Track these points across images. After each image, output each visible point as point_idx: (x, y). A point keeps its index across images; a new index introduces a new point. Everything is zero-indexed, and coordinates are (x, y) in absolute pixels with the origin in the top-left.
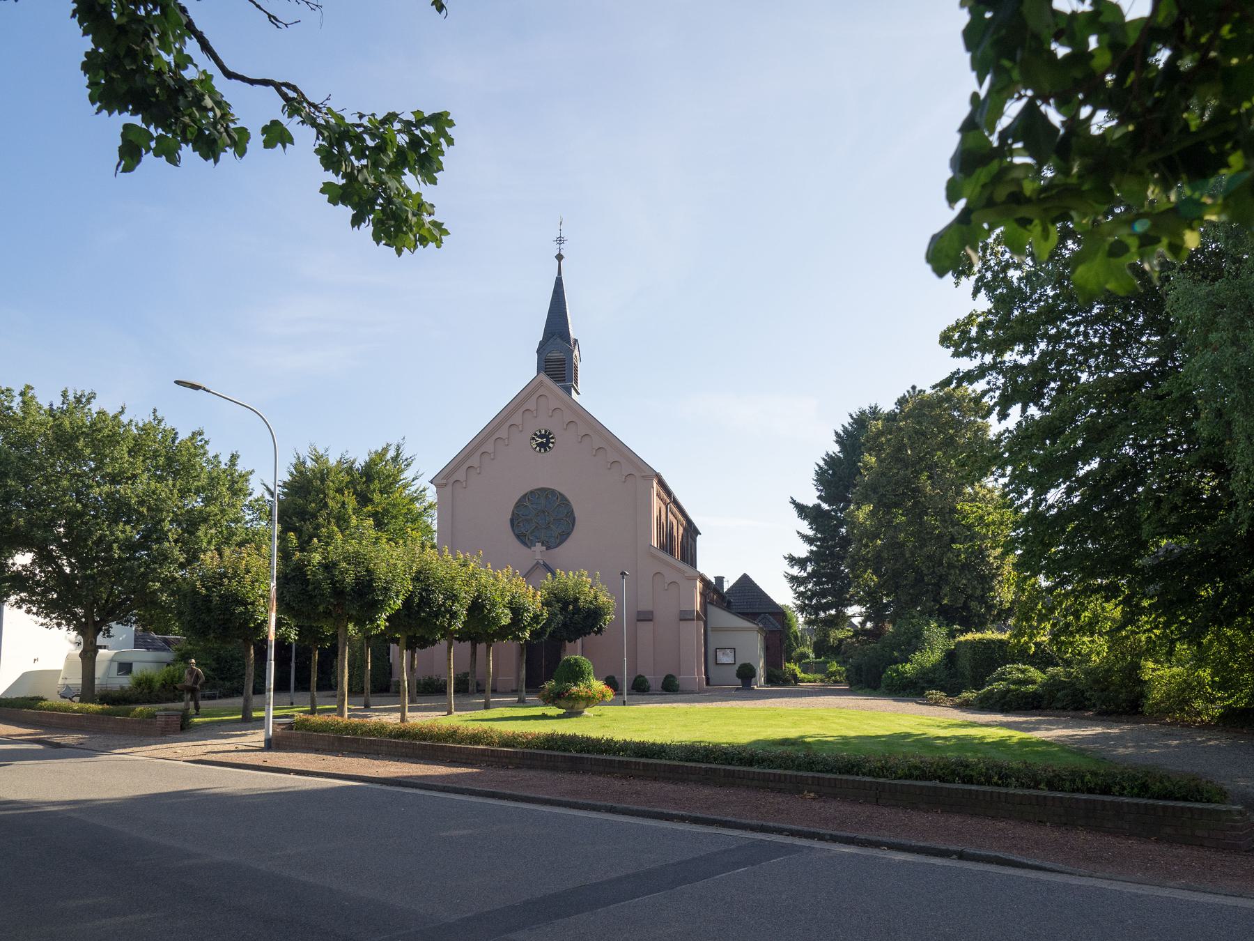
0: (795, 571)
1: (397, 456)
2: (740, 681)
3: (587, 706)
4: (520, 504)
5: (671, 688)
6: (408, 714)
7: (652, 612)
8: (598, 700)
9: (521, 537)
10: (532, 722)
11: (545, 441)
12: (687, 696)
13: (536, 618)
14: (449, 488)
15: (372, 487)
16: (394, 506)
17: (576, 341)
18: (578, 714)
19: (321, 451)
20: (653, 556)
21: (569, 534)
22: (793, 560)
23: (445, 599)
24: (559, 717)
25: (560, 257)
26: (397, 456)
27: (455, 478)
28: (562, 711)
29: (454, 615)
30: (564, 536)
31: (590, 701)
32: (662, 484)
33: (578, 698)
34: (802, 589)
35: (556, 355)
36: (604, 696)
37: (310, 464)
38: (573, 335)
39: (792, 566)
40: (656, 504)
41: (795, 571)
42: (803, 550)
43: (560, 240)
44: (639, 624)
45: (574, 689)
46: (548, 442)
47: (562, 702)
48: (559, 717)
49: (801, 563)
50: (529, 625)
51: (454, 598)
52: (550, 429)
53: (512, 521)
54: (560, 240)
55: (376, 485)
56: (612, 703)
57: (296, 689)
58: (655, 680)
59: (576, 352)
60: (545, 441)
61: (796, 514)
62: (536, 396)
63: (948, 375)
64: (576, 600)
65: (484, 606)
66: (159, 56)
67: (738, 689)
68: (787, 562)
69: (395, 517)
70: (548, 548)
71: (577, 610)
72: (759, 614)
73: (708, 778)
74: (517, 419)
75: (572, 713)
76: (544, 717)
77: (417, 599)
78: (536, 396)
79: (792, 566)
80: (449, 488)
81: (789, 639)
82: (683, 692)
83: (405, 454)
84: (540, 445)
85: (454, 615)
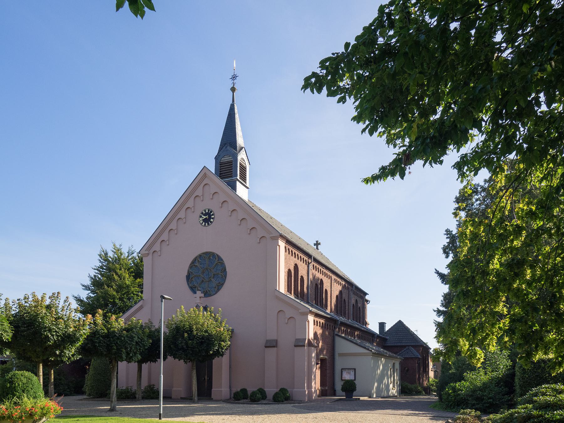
2: (344, 393)
7: (276, 341)
9: (193, 289)
11: (208, 217)
19: (118, 247)
21: (223, 284)
25: (233, 90)
27: (154, 249)
32: (288, 242)
35: (226, 159)
37: (111, 254)
39: (439, 316)
43: (234, 77)
44: (266, 349)
46: (210, 218)
53: (188, 278)
54: (234, 77)
58: (271, 390)
60: (208, 217)
61: (440, 281)
64: (191, 330)
66: (464, 256)
68: (435, 313)
70: (207, 294)
71: (191, 337)
72: (405, 346)
74: (190, 204)
80: (150, 256)
84: (205, 220)
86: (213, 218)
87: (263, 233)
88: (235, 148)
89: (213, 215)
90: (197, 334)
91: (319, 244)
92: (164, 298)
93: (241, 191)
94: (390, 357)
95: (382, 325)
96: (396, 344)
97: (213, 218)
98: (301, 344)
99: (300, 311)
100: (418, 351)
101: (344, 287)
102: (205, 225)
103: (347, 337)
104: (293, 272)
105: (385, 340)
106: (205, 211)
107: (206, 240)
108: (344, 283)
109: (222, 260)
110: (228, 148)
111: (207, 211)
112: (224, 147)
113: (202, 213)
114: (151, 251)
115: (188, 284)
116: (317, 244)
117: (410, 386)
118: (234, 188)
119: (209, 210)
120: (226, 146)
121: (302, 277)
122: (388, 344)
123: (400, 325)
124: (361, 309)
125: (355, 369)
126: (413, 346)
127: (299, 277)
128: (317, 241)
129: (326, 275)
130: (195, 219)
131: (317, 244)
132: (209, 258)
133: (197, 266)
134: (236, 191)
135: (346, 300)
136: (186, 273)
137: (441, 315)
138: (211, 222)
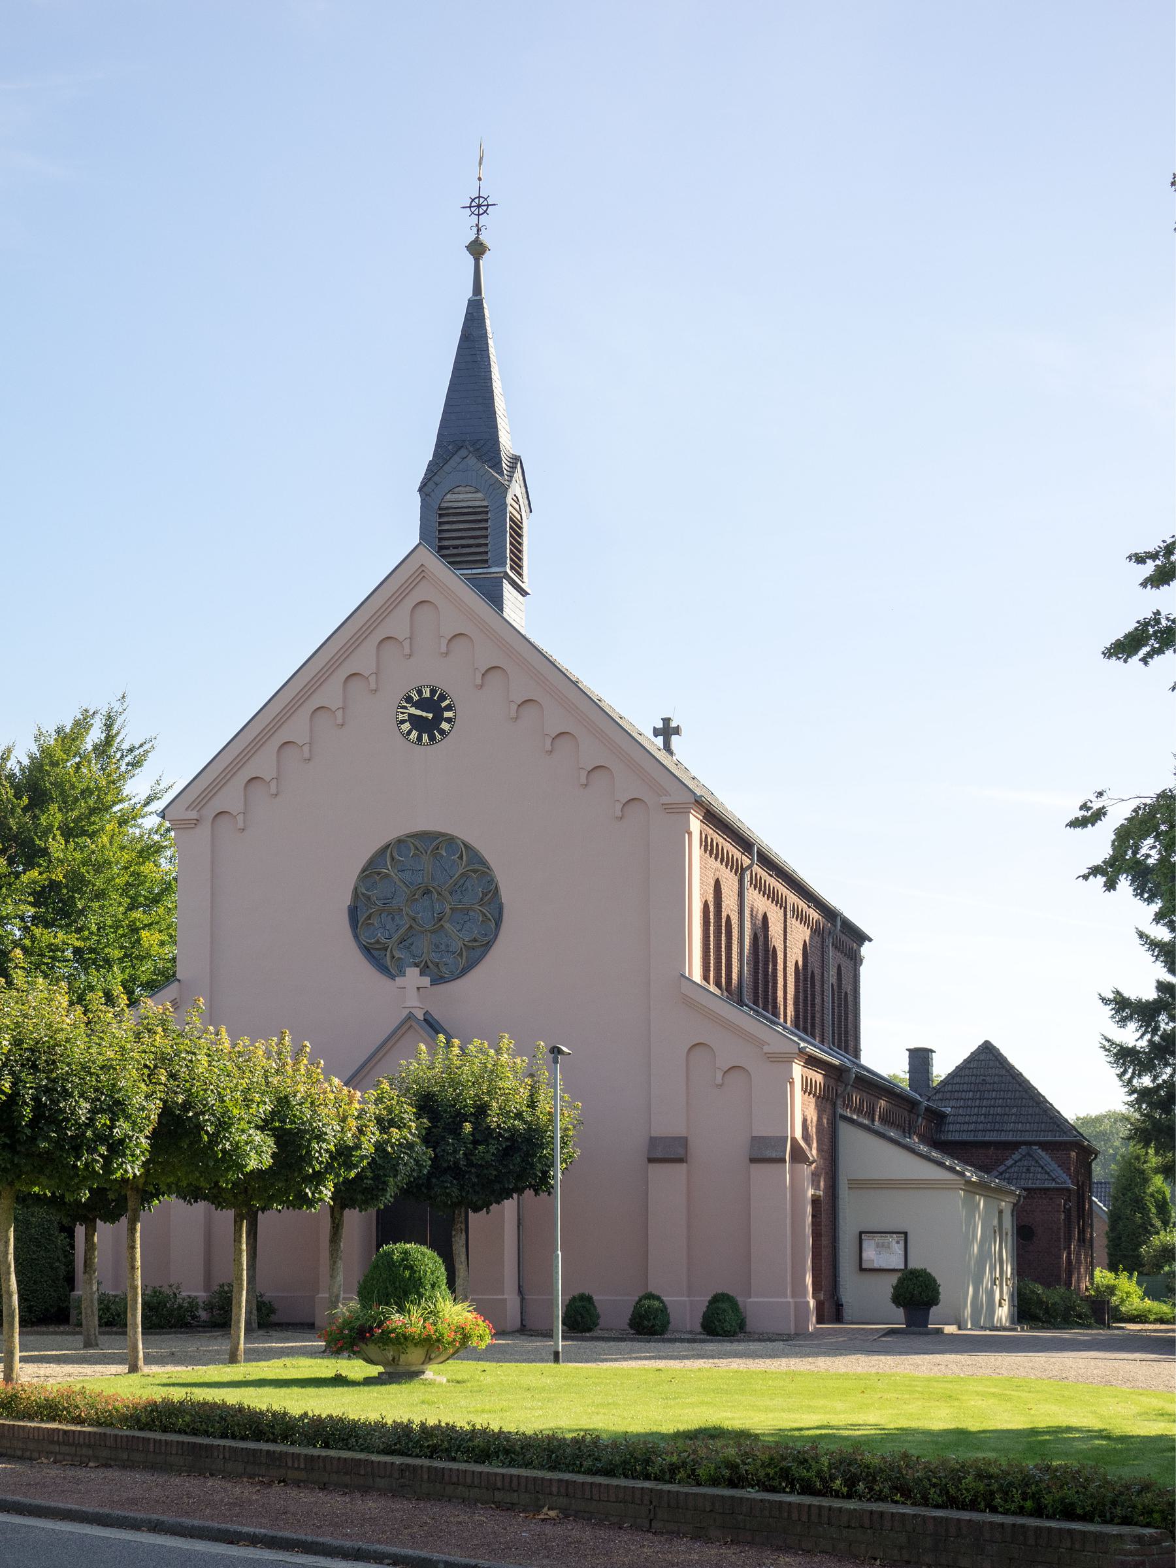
0: (1131, 1035)
1: (109, 741)
2: (901, 1311)
3: (428, 1359)
4: (371, 871)
5: (724, 1324)
6: (17, 1365)
7: (684, 1142)
8: (461, 1346)
9: (374, 953)
10: (311, 1391)
11: (429, 716)
12: (753, 1346)
13: (343, 1154)
14: (205, 830)
15: (44, 820)
16: (99, 868)
17: (516, 460)
18: (412, 1375)
20: (689, 1003)
21: (488, 946)
22: (1123, 1007)
23: (94, 1112)
24: (368, 1382)
25: (477, 249)
26: (109, 741)
27: (217, 805)
28: (374, 1370)
29: (117, 1148)
30: (477, 950)
31: (432, 1347)
32: (715, 819)
33: (403, 1340)
34: (1146, 1081)
35: (464, 498)
36: (466, 1337)
38: (508, 442)
39: (1123, 1022)
40: (700, 873)
41: (1131, 1035)
42: (1144, 978)
43: (479, 206)
45: (397, 1320)
46: (439, 718)
47: (372, 1350)
48: (368, 1382)
49: (1145, 1013)
50: (329, 1167)
51: (117, 1108)
52: (444, 685)
53: (353, 912)
54: (479, 206)
55: (53, 816)
56: (491, 1355)
57: (247, 1360)
58: (685, 1305)
59: (516, 488)
60: (429, 716)
62: (410, 603)
63: (1130, 626)
64: (482, 1110)
65: (200, 1127)
67: (892, 1332)
68: (1108, 1011)
69: (100, 895)
70: (438, 980)
71: (484, 1134)
72: (1016, 1145)
73: (404, 1485)
74: (363, 660)
75: (397, 1374)
76: (339, 1381)
77: (27, 1112)
78: (410, 603)
79: (1123, 1022)
80: (205, 830)
81: (1144, 1209)
82: (751, 1337)
83: (129, 737)
85: (117, 1148)
86: (449, 720)
87: (634, 786)
88: (496, 464)
89: (449, 708)
90: (499, 1126)
91: (677, 731)
92: (560, 1051)
93: (514, 607)
94: (998, 1190)
95: (920, 1059)
96: (980, 1137)
97: (449, 720)
98: (774, 1155)
99: (766, 1049)
100: (1064, 1165)
101: (817, 931)
102: (420, 739)
103: (861, 1120)
104: (712, 908)
105: (937, 1118)
106: (420, 692)
107: (427, 792)
108: (814, 915)
109: (483, 862)
110: (472, 461)
111: (427, 694)
112: (456, 458)
113: (409, 699)
114: (210, 812)
115: (356, 937)
116: (667, 731)
117: (1053, 1296)
118: (496, 601)
119: (433, 692)
120: (463, 452)
121: (728, 917)
122: (953, 1134)
123: (987, 1063)
124: (850, 998)
125: (906, 1234)
126: (1044, 1145)
127: (724, 921)
128: (666, 721)
129: (780, 902)
130: (381, 712)
131: (667, 731)
132: (435, 854)
133: (387, 876)
134: (501, 610)
135: (817, 971)
136: (347, 900)
137: (1130, 1018)
138: (442, 732)
